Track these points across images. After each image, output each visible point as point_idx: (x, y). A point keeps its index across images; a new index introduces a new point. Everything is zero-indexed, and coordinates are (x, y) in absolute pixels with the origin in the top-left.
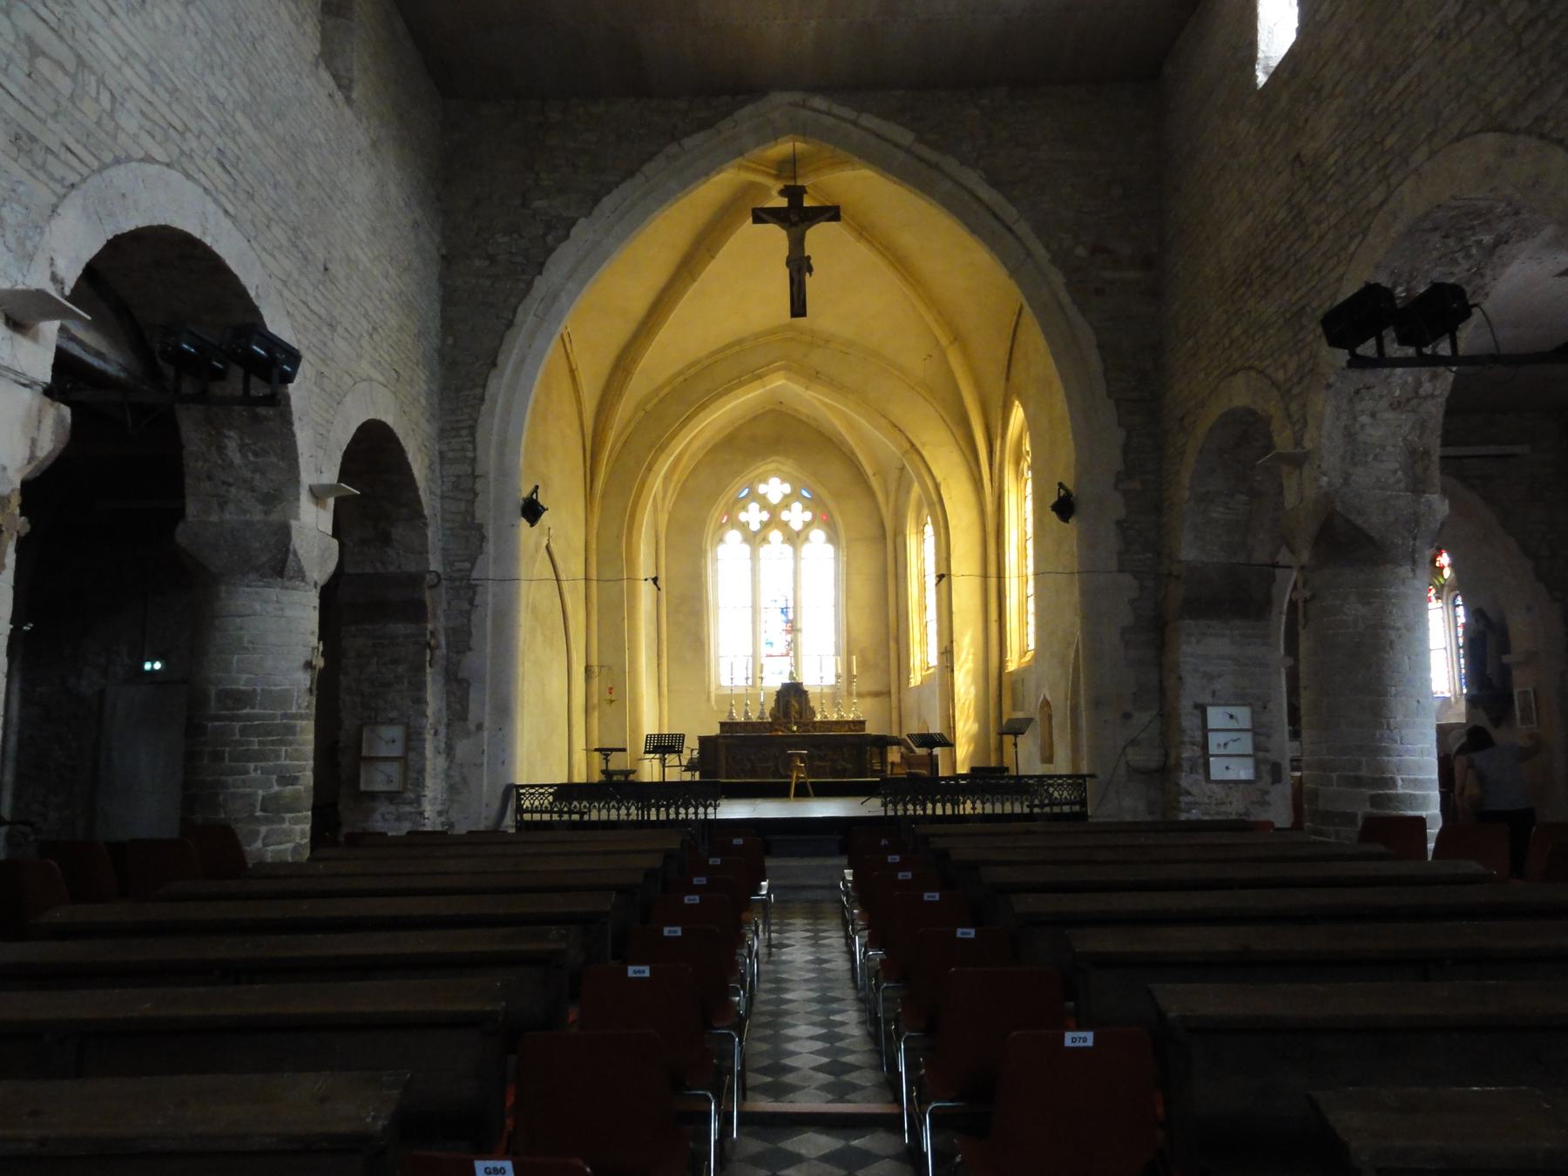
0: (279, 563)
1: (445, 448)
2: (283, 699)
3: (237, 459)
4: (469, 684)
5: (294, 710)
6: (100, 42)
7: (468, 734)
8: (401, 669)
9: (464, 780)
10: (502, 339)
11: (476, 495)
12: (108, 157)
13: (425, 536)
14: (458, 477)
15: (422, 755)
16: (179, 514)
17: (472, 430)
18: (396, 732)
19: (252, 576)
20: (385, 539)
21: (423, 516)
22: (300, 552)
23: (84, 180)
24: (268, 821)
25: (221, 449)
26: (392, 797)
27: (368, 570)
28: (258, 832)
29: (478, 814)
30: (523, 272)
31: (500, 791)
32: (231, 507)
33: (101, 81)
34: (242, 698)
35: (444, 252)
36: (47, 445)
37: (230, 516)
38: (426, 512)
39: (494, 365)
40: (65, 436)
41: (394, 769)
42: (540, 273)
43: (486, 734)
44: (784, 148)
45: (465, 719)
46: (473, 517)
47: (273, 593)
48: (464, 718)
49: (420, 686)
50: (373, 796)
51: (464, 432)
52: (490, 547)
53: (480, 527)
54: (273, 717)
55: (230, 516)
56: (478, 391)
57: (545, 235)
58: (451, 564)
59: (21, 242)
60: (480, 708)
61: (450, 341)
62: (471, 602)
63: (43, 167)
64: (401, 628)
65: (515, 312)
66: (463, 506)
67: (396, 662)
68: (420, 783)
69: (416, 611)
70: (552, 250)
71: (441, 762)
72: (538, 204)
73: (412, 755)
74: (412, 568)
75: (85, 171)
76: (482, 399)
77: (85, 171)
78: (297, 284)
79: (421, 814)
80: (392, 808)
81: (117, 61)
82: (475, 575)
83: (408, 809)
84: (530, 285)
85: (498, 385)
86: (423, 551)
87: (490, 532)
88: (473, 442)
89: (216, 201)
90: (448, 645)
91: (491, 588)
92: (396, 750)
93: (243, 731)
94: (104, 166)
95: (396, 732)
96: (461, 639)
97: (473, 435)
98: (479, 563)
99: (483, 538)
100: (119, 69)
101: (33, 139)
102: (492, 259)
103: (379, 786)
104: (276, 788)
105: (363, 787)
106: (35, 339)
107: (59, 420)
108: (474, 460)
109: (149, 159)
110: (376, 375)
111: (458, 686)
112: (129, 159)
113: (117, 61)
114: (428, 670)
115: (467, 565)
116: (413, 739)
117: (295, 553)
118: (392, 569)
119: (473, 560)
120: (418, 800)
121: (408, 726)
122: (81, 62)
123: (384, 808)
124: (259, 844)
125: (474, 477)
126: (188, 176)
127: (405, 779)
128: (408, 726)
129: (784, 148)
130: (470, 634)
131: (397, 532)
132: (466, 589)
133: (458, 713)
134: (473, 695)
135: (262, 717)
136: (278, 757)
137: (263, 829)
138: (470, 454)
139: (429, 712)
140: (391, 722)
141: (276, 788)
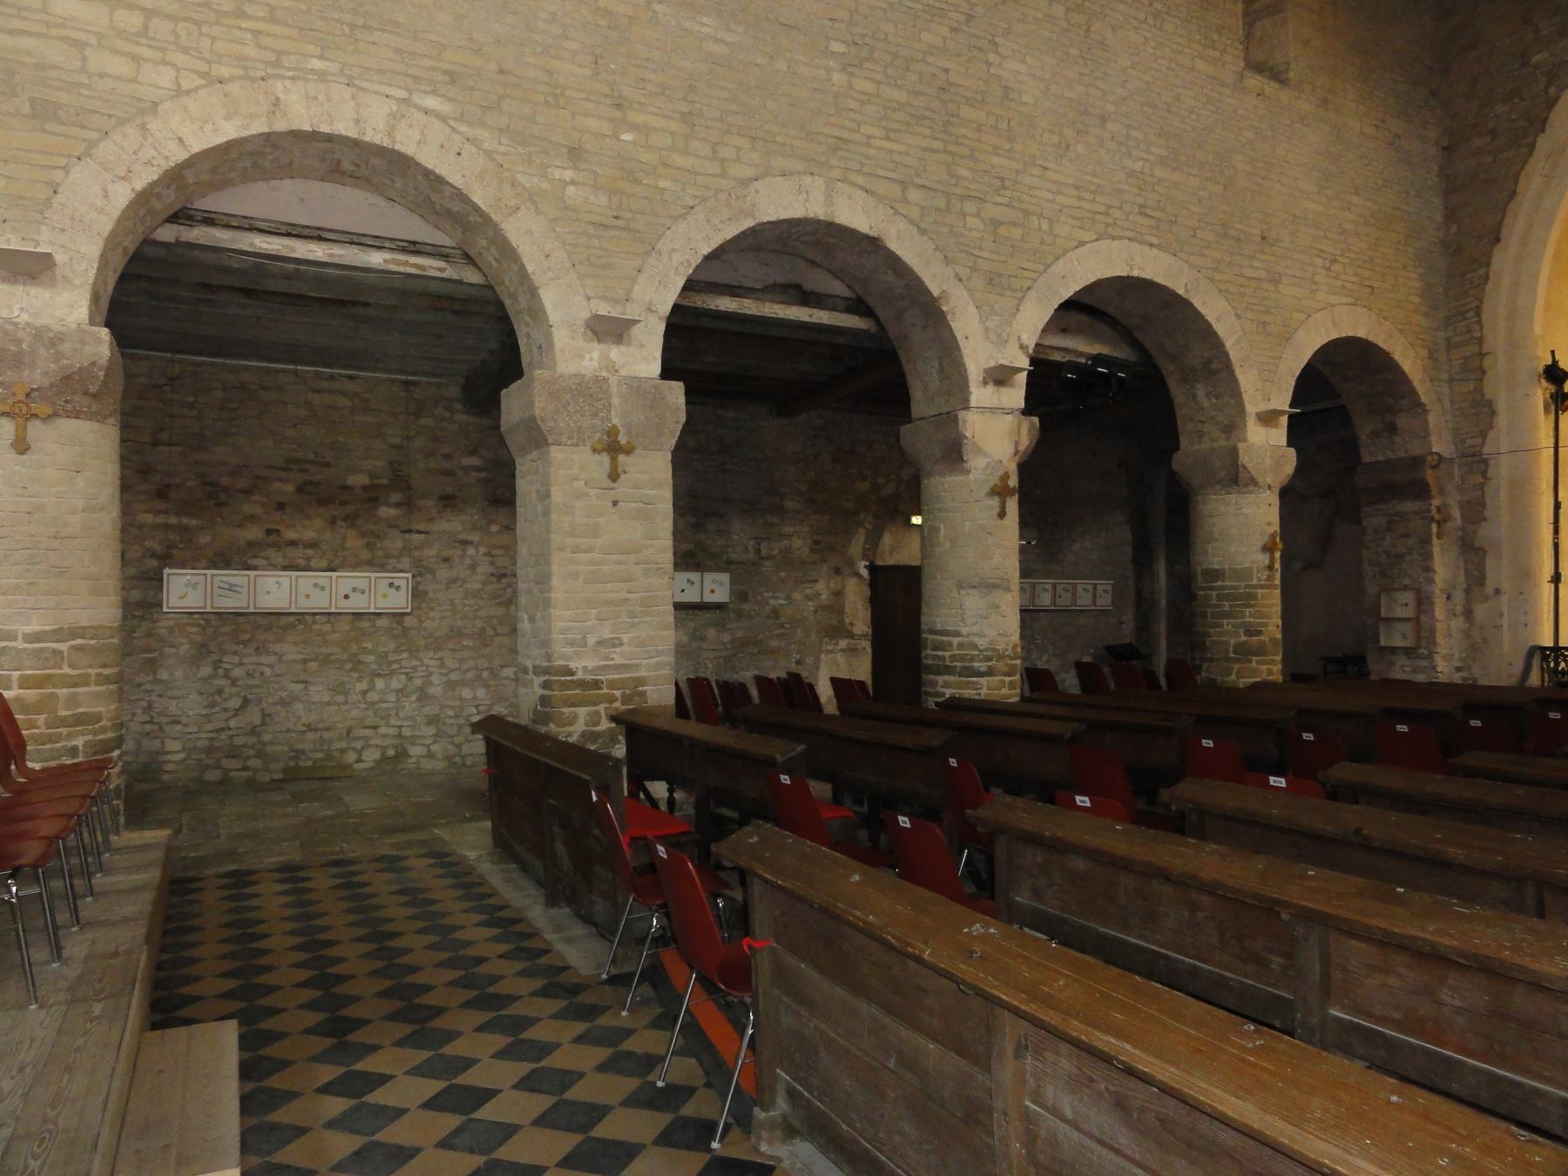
0: (1236, 478)
1: (1450, 334)
2: (1244, 574)
3: (1205, 403)
4: (1485, 552)
5: (1255, 582)
6: (1037, 192)
7: (1486, 598)
8: (1410, 542)
9: (1485, 641)
10: (1504, 212)
11: (1484, 373)
12: (1050, 259)
13: (1427, 422)
14: (1466, 358)
15: (1432, 617)
16: (1177, 448)
17: (1478, 311)
18: (1408, 597)
19: (1218, 487)
20: (1392, 429)
21: (1422, 405)
22: (1249, 466)
23: (1035, 281)
24: (1237, 661)
25: (1194, 397)
26: (1409, 652)
27: (1381, 458)
28: (1231, 669)
29: (1502, 668)
30: (1525, 136)
31: (1523, 653)
32: (1205, 439)
33: (1041, 216)
34: (1216, 575)
35: (1446, 143)
36: (1025, 442)
37: (1206, 444)
38: (1424, 400)
39: (1498, 240)
40: (1036, 434)
41: (1408, 628)
42: (1543, 130)
43: (1504, 599)
44: (361, 765)
45: (1483, 585)
46: (1482, 395)
47: (1233, 498)
48: (1480, 581)
49: (1427, 556)
50: (1394, 650)
51: (1471, 314)
52: (1502, 420)
53: (1490, 404)
54: (1237, 588)
55: (1206, 444)
56: (1482, 271)
57: (1547, 87)
58: (1463, 441)
59: (999, 336)
60: (1498, 572)
61: (1454, 229)
62: (1484, 474)
63: (1009, 288)
64: (1409, 506)
65: (1516, 182)
66: (1471, 386)
67: (1407, 536)
68: (1432, 641)
69: (1421, 491)
70: (1557, 99)
71: (1458, 624)
72: (1537, 58)
73: (1423, 617)
74: (1417, 452)
75: (1034, 275)
76: (1487, 278)
77: (1034, 275)
78: (1230, 264)
79: (1434, 668)
80: (1408, 662)
81: (1050, 196)
82: (1487, 450)
83: (1423, 663)
84: (1532, 147)
85: (1502, 259)
86: (1425, 436)
87: (1501, 406)
88: (1480, 322)
89: (1139, 242)
90: (1464, 517)
91: (1504, 460)
92: (1409, 612)
93: (1219, 597)
94: (1047, 266)
95: (1408, 597)
96: (1475, 511)
97: (1478, 315)
98: (1489, 437)
99: (1493, 413)
100: (1053, 201)
101: (1000, 275)
102: (1493, 133)
103: (1398, 642)
104: (1244, 638)
105: (1383, 643)
106: (1012, 386)
107: (1032, 424)
108: (1480, 340)
109: (1082, 244)
110: (1333, 299)
111: (1473, 554)
112: (1066, 251)
113: (1050, 196)
114: (1435, 541)
115: (1478, 441)
116: (1423, 602)
117: (1244, 467)
118: (1401, 454)
119: (1483, 435)
120: (1430, 657)
121: (1418, 591)
122: (1027, 213)
123: (1402, 660)
124: (1233, 677)
125: (1482, 355)
126: (1113, 238)
127: (1418, 637)
128: (1418, 591)
129: (361, 765)
130: (1484, 505)
131: (1402, 422)
132: (1477, 462)
133: (1476, 579)
134: (1490, 564)
135: (1230, 588)
136: (1243, 616)
137: (1236, 667)
138: (1477, 335)
139: (1437, 579)
140: (1406, 588)
141: (1244, 638)
